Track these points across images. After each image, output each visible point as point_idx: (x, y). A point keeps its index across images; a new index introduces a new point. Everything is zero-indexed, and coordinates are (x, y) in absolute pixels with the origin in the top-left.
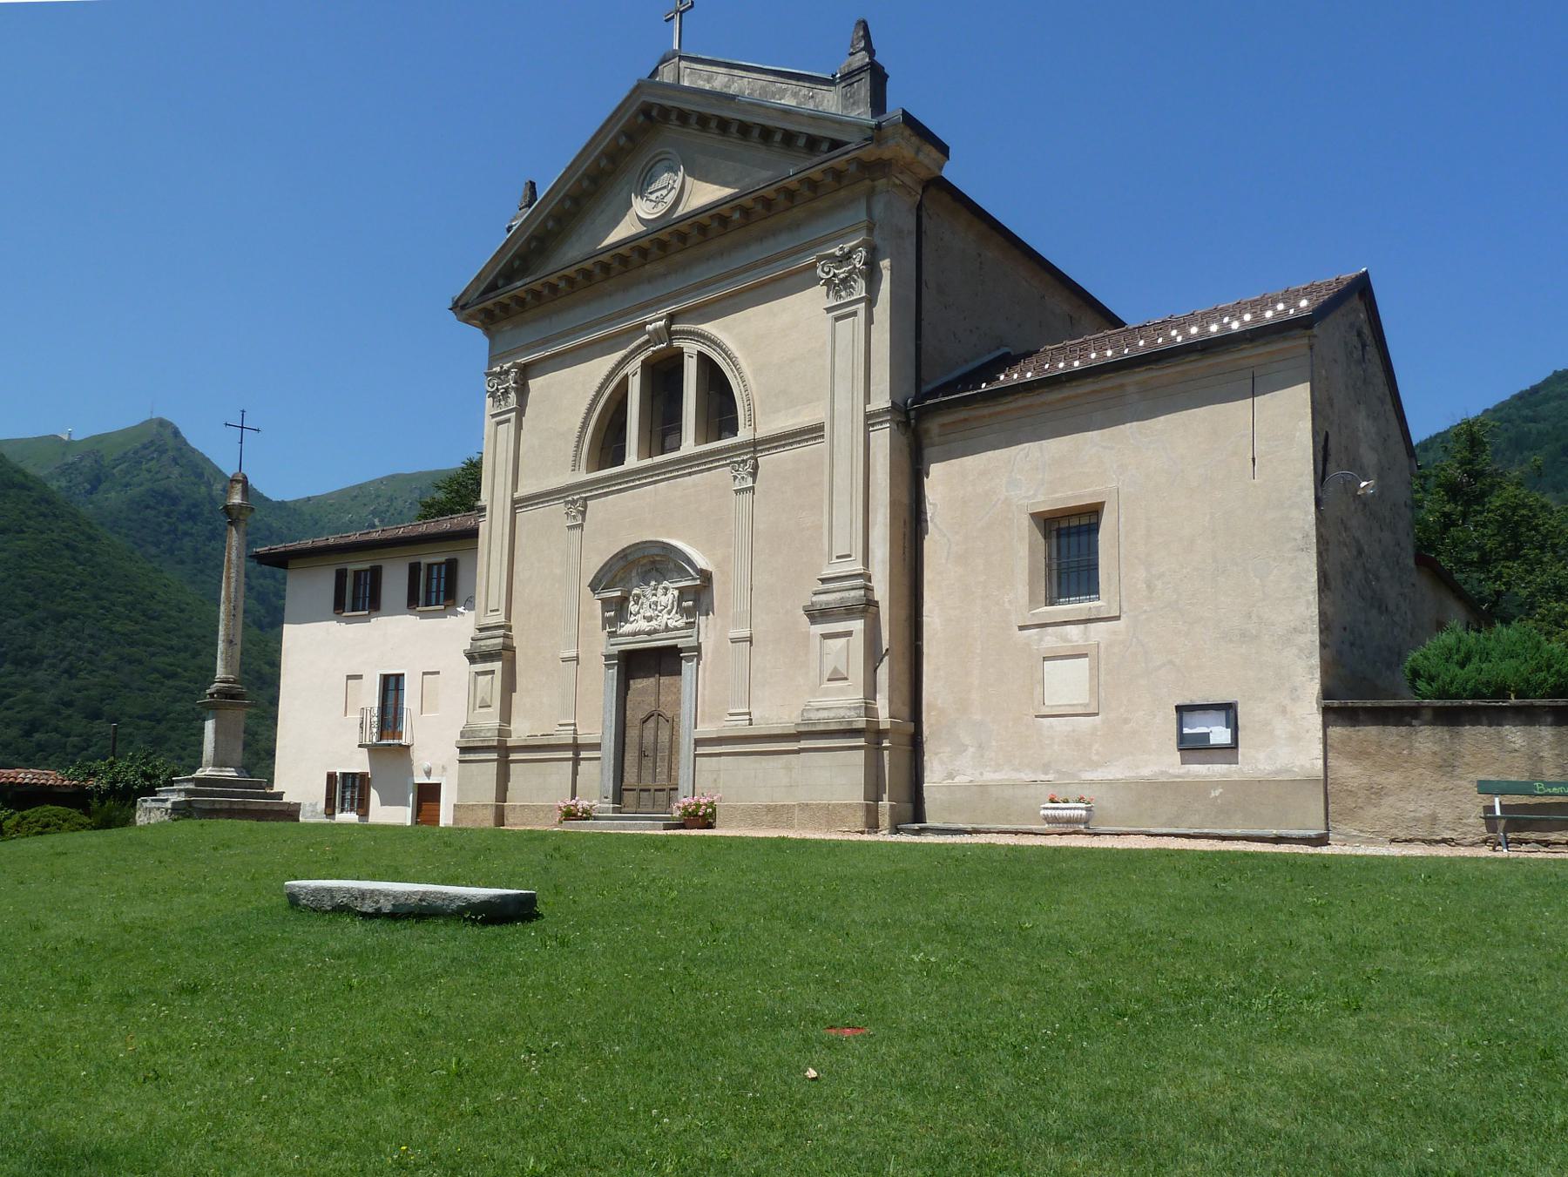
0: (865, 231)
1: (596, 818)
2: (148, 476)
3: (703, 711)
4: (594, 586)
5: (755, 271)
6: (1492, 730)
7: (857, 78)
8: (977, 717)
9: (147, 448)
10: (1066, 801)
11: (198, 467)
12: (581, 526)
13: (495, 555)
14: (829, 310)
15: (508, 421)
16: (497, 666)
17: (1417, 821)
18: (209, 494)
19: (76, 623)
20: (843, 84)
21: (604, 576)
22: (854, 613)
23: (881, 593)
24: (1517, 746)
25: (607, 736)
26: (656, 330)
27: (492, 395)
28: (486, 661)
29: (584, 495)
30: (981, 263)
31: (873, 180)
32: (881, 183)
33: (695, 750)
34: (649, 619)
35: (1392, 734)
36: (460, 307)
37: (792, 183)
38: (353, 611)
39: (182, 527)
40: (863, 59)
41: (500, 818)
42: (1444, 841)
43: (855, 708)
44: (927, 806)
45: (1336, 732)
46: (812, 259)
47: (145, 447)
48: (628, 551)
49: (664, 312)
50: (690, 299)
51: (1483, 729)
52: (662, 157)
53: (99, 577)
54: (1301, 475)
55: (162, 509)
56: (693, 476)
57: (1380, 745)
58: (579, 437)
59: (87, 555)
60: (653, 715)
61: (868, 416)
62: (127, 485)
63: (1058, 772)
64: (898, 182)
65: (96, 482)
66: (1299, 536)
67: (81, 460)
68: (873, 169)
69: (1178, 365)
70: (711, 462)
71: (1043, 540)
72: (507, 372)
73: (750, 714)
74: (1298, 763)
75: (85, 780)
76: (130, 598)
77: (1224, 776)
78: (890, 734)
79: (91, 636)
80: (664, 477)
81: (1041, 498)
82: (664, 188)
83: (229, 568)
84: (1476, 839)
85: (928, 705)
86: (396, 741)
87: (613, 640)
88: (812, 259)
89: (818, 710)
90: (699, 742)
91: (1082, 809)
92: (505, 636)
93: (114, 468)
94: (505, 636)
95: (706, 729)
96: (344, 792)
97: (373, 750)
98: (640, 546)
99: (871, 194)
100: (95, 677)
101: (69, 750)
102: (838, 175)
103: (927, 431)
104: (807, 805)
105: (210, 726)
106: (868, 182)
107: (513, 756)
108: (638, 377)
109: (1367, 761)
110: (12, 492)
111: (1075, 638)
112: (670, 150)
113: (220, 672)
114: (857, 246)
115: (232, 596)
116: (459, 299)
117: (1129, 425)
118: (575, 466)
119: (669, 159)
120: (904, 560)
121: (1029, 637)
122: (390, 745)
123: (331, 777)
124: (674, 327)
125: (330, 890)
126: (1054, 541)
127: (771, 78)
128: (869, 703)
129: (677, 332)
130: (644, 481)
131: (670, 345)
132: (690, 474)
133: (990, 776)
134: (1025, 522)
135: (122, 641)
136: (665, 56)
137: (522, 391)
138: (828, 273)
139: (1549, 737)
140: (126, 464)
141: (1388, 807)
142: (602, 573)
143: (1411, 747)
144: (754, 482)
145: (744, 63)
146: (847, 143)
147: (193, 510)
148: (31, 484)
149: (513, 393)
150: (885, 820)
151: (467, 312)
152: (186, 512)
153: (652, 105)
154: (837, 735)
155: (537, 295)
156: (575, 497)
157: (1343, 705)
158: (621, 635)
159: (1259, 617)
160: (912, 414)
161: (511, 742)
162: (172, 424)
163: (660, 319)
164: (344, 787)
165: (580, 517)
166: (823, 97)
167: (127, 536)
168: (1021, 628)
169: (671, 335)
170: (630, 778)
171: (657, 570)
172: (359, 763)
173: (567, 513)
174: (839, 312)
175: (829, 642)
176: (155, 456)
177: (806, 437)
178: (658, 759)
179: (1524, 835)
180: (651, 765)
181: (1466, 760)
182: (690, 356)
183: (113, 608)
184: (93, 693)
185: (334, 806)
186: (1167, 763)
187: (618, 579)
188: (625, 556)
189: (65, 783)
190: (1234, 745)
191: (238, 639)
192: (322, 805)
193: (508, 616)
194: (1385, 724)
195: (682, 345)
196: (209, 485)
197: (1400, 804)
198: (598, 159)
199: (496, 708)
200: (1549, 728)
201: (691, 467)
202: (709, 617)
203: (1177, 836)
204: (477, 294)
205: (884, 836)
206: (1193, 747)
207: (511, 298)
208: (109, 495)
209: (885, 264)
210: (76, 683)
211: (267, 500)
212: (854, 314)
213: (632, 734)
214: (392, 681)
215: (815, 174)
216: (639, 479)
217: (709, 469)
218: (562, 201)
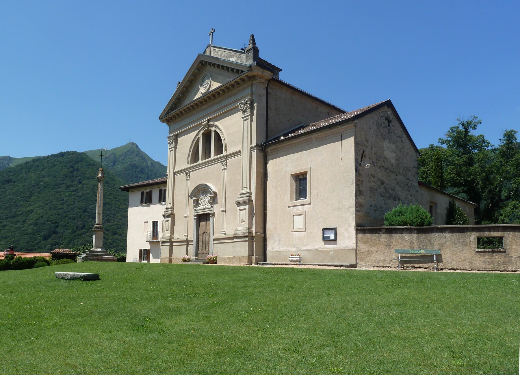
0: (250, 96)
1: (191, 261)
2: (129, 160)
3: (215, 231)
4: (191, 196)
5: (226, 108)
6: (400, 235)
7: (250, 51)
8: (279, 232)
9: (129, 152)
10: (295, 256)
11: (143, 157)
12: (189, 179)
13: (170, 188)
14: (242, 118)
15: (173, 150)
16: (170, 219)
17: (380, 261)
18: (147, 165)
19: (109, 206)
20: (247, 53)
21: (193, 193)
22: (246, 203)
23: (254, 198)
24: (407, 240)
25: (194, 238)
26: (205, 124)
27: (169, 143)
28: (167, 218)
29: (189, 171)
30: (292, 100)
31: (252, 81)
32: (254, 82)
33: (213, 242)
34: (203, 205)
35: (374, 236)
36: (161, 118)
37: (233, 83)
38: (146, 203)
39: (139, 175)
40: (251, 46)
41: (170, 260)
42: (387, 267)
43: (246, 230)
44: (267, 257)
45: (360, 236)
46: (238, 104)
47: (128, 151)
48: (198, 187)
49: (206, 119)
50: (213, 115)
51: (398, 235)
52: (206, 75)
53: (115, 192)
54: (352, 163)
55: (133, 170)
57: (371, 239)
58: (188, 155)
59: (112, 185)
61: (251, 148)
62: (124, 163)
63: (296, 247)
64: (259, 81)
65: (114, 162)
66: (351, 180)
67: (110, 156)
68: (252, 78)
69: (324, 132)
70: (217, 161)
71: (295, 182)
72: (172, 136)
73: (225, 232)
74: (350, 245)
75: (77, 252)
76: (124, 198)
77: (333, 248)
78: (255, 237)
79: (114, 210)
81: (293, 170)
82: (207, 84)
83: (98, 194)
84: (395, 266)
85: (268, 229)
86: (156, 240)
87: (196, 212)
88: (238, 104)
89: (238, 230)
90: (214, 240)
91: (298, 258)
92: (172, 211)
93: (119, 158)
94: (172, 211)
95: (216, 236)
96: (144, 255)
97: (151, 243)
99: (252, 85)
100: (115, 222)
101: (108, 244)
102: (243, 80)
103: (268, 151)
104: (235, 257)
105: (94, 236)
106: (250, 82)
107: (174, 244)
108: (202, 137)
109: (368, 244)
110: (90, 167)
111: (300, 210)
112: (208, 73)
113: (97, 222)
114: (248, 100)
115: (99, 202)
116: (160, 116)
117: (313, 149)
119: (207, 76)
120: (261, 188)
121: (290, 209)
122: (154, 241)
123: (140, 250)
124: (209, 123)
125: (61, 274)
126: (298, 182)
127: (231, 52)
128: (250, 229)
131: (208, 128)
132: (212, 165)
133: (282, 249)
134: (289, 177)
135: (122, 211)
136: (208, 46)
137: (176, 142)
138: (242, 108)
139: (416, 237)
140: (123, 157)
141: (373, 257)
143: (379, 240)
144: (226, 167)
145: (225, 48)
146: (244, 71)
147: (142, 170)
148: (96, 164)
149: (174, 142)
150: (254, 261)
151: (162, 120)
152: (140, 171)
153: (202, 61)
154: (242, 238)
155: (178, 114)
157: (361, 228)
159: (342, 204)
160: (263, 147)
161: (173, 240)
162: (136, 144)
163: (205, 121)
164: (144, 253)
165: (188, 177)
166: (243, 57)
167: (124, 179)
168: (289, 207)
169: (208, 125)
170: (200, 250)
172: (147, 247)
173: (186, 176)
174: (245, 119)
175: (241, 211)
176: (131, 154)
177: (238, 154)
179: (408, 265)
181: (393, 244)
183: (120, 201)
184: (114, 227)
185: (141, 259)
186: (320, 245)
187: (196, 194)
188: (197, 188)
189: (71, 253)
190: (336, 239)
191: (101, 213)
193: (173, 205)
194: (372, 233)
195: (211, 128)
196: (147, 162)
197: (376, 256)
198: (191, 76)
199: (169, 231)
200: (416, 234)
201: (212, 163)
202: (217, 205)
203: (319, 265)
204: (164, 115)
205: (253, 265)
206: (326, 240)
207: (172, 116)
208: (118, 166)
209: (255, 105)
210: (110, 224)
211: (164, 166)
212: (248, 119)
213: (201, 237)
214: (156, 222)
215: (237, 80)
217: (217, 163)
218: (183, 88)
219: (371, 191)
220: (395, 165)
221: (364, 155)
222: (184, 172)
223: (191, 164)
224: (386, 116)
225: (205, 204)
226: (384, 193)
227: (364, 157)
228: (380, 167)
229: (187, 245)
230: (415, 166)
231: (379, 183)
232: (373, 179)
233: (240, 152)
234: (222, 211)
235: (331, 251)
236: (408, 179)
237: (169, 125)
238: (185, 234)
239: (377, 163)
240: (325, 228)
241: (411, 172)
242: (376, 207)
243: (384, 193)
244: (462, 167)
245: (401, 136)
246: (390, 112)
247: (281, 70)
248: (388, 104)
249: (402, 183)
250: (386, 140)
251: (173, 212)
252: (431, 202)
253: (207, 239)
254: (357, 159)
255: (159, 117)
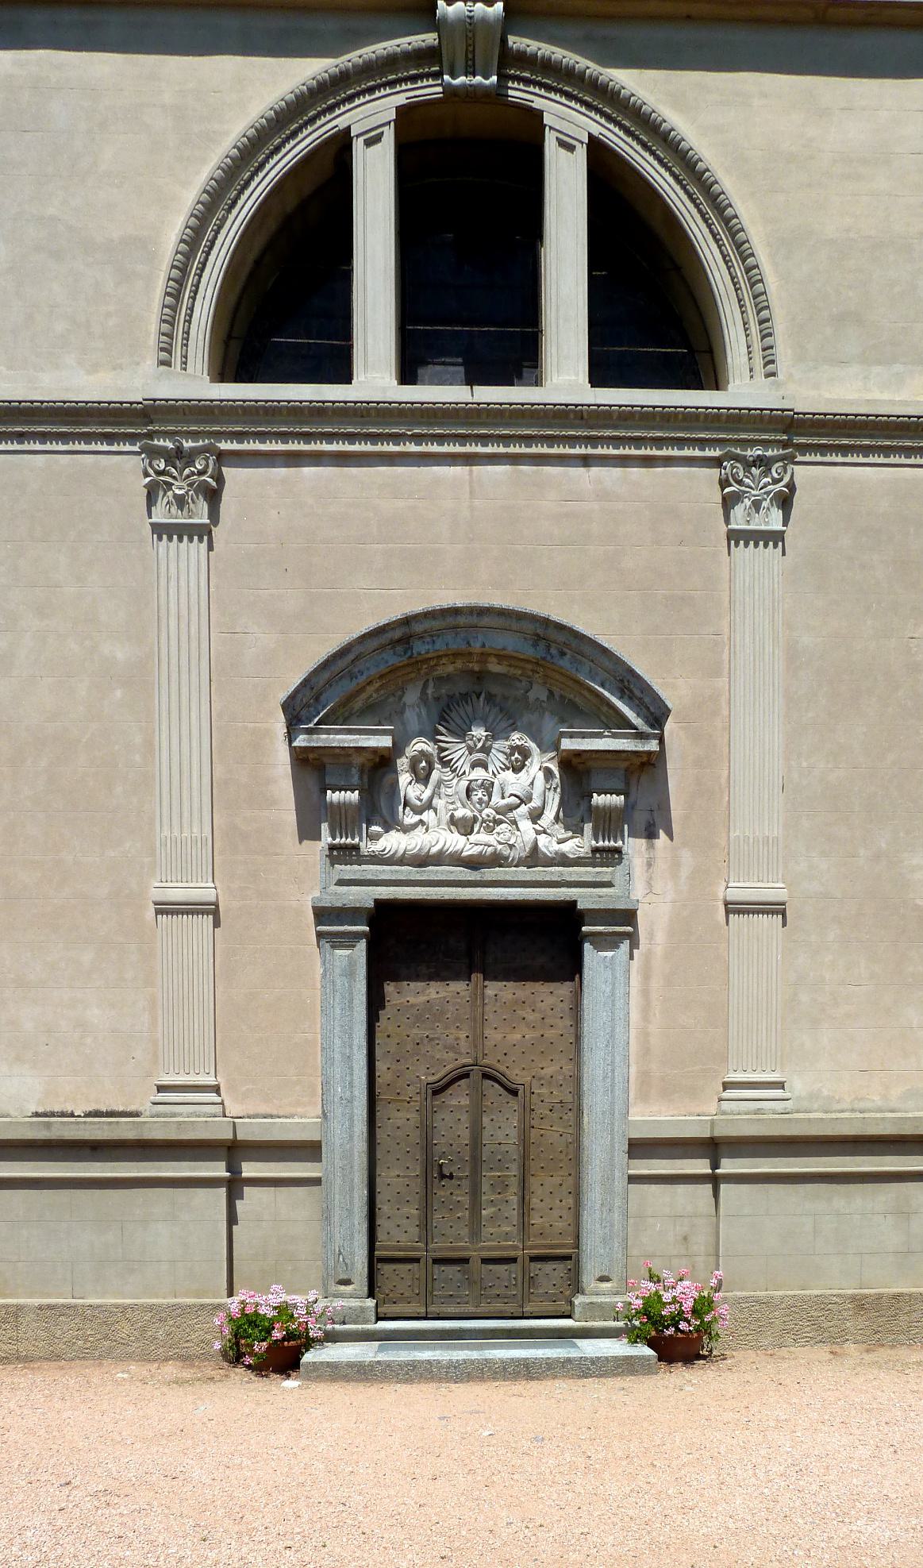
29: (225, 446)
34: (465, 827)
48: (418, 628)
56: (595, 471)
60: (466, 1076)
70: (658, 442)
80: (502, 450)
90: (639, 1148)
98: (462, 620)
105: (626, 827)
129: (525, 60)
130: (435, 448)
132: (586, 461)
142: (326, 675)
156: (188, 444)
158: (377, 859)
171: (490, 698)
178: (485, 1187)
180: (466, 1200)
182: (562, 144)
187: (358, 704)
188: (406, 641)
216: (418, 439)
217: (648, 462)
222: (132, 438)
238: (167, 1080)
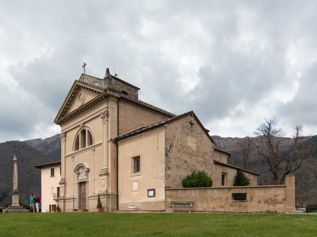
4: (74, 171)
14: (102, 122)
16: (63, 185)
23: (110, 171)
61: (108, 141)
63: (134, 201)
81: (132, 155)
87: (78, 181)
90: (88, 197)
95: (90, 195)
118: (73, 151)
119: (82, 95)
120: (115, 166)
123: (50, 206)
133: (127, 202)
134: (130, 159)
161: (66, 198)
170: (81, 204)
192: (49, 210)
199: (63, 193)
212: (105, 123)
219: (177, 167)
220: (195, 151)
221: (172, 145)
223: (75, 151)
224: (190, 121)
225: (82, 177)
226: (187, 168)
227: (172, 147)
228: (184, 153)
229: (74, 201)
230: (211, 151)
231: (183, 162)
232: (178, 160)
233: (101, 144)
234: (92, 180)
235: (152, 202)
236: (206, 159)
237: (61, 126)
239: (182, 150)
240: (149, 189)
241: (208, 155)
242: (181, 177)
243: (187, 168)
244: (287, 148)
245: (201, 133)
246: (192, 119)
247: (140, 89)
248: (191, 114)
249: (201, 162)
250: (189, 136)
251: (65, 181)
252: (223, 173)
253: (85, 198)
254: (167, 148)
255: (54, 121)
